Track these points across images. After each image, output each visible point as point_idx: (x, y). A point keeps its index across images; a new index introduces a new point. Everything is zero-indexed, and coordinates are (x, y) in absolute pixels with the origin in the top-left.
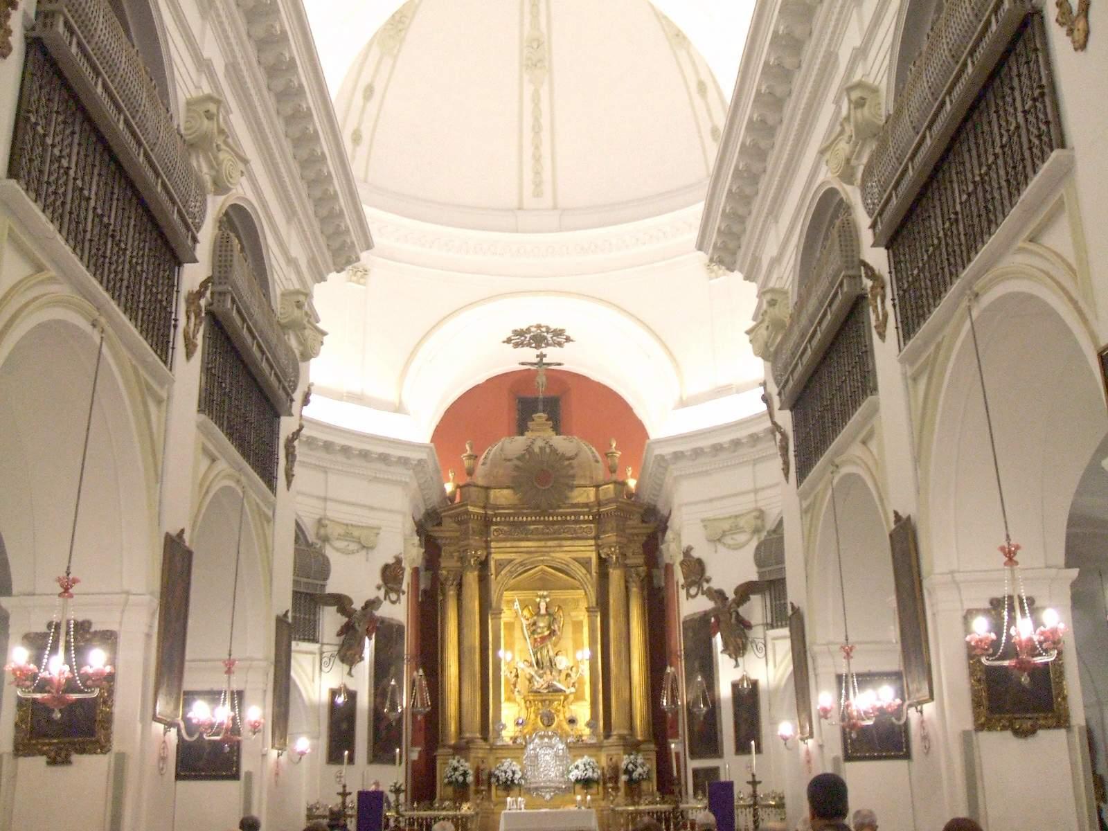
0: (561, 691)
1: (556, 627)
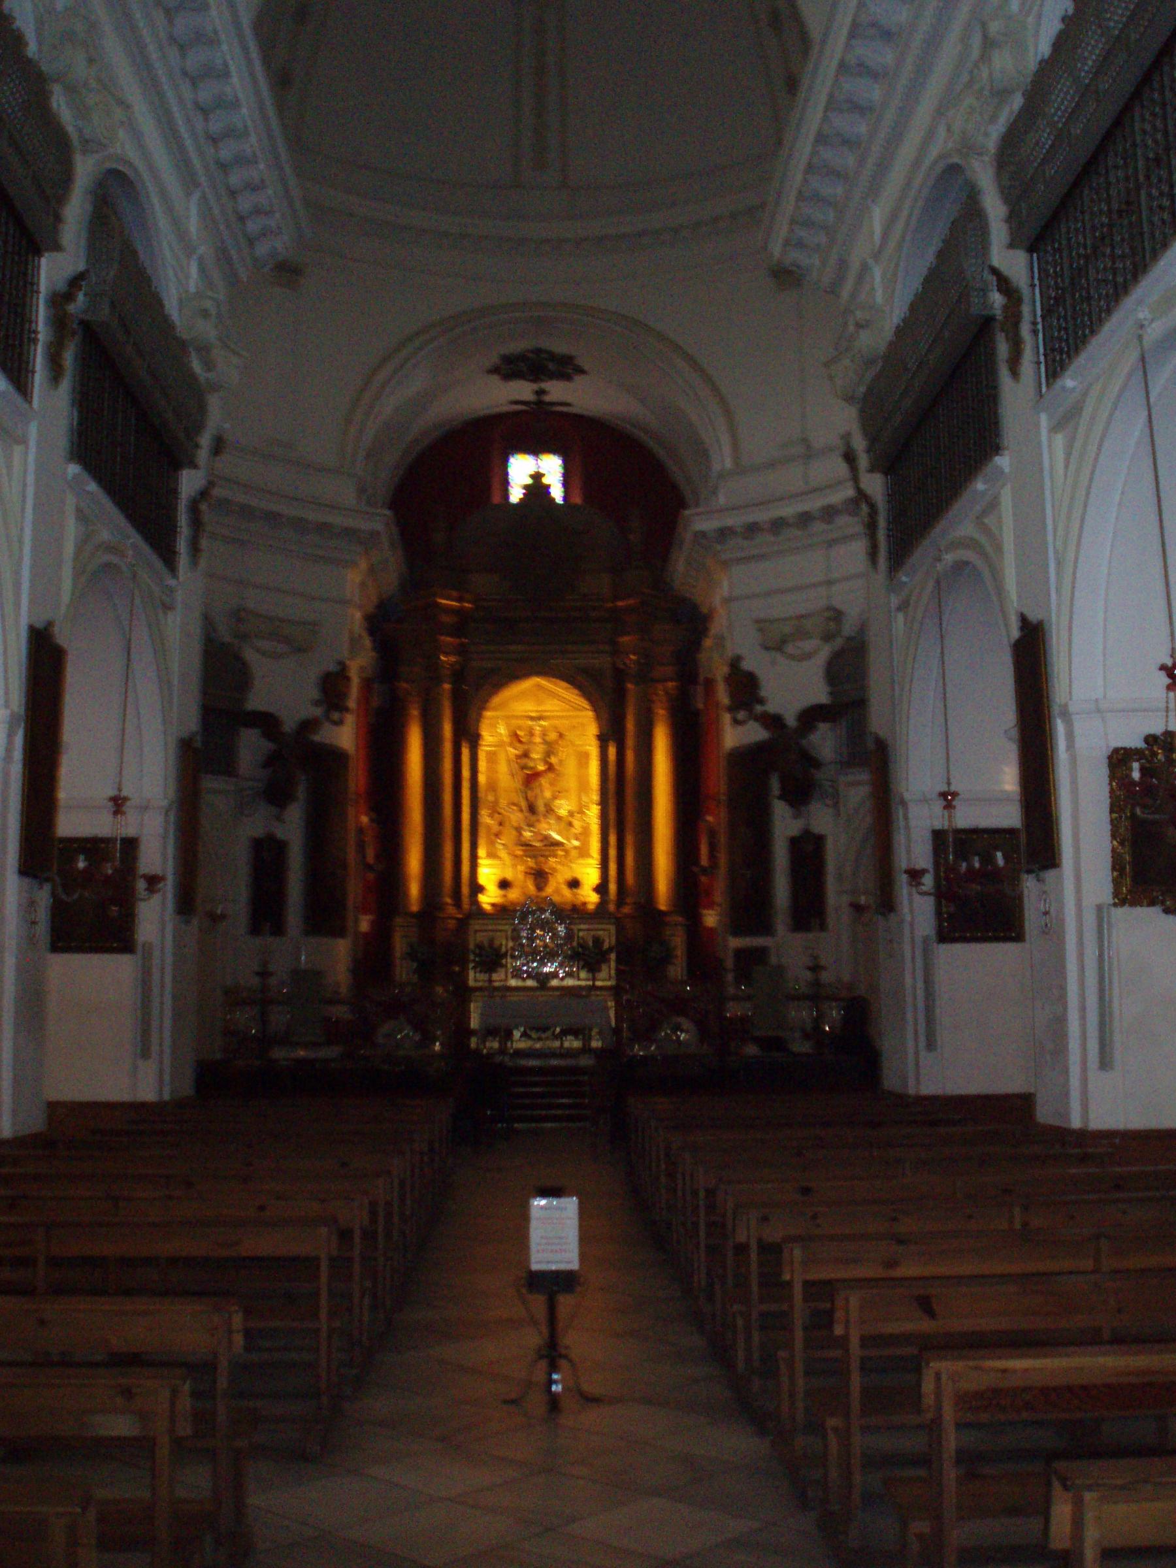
1: (553, 760)
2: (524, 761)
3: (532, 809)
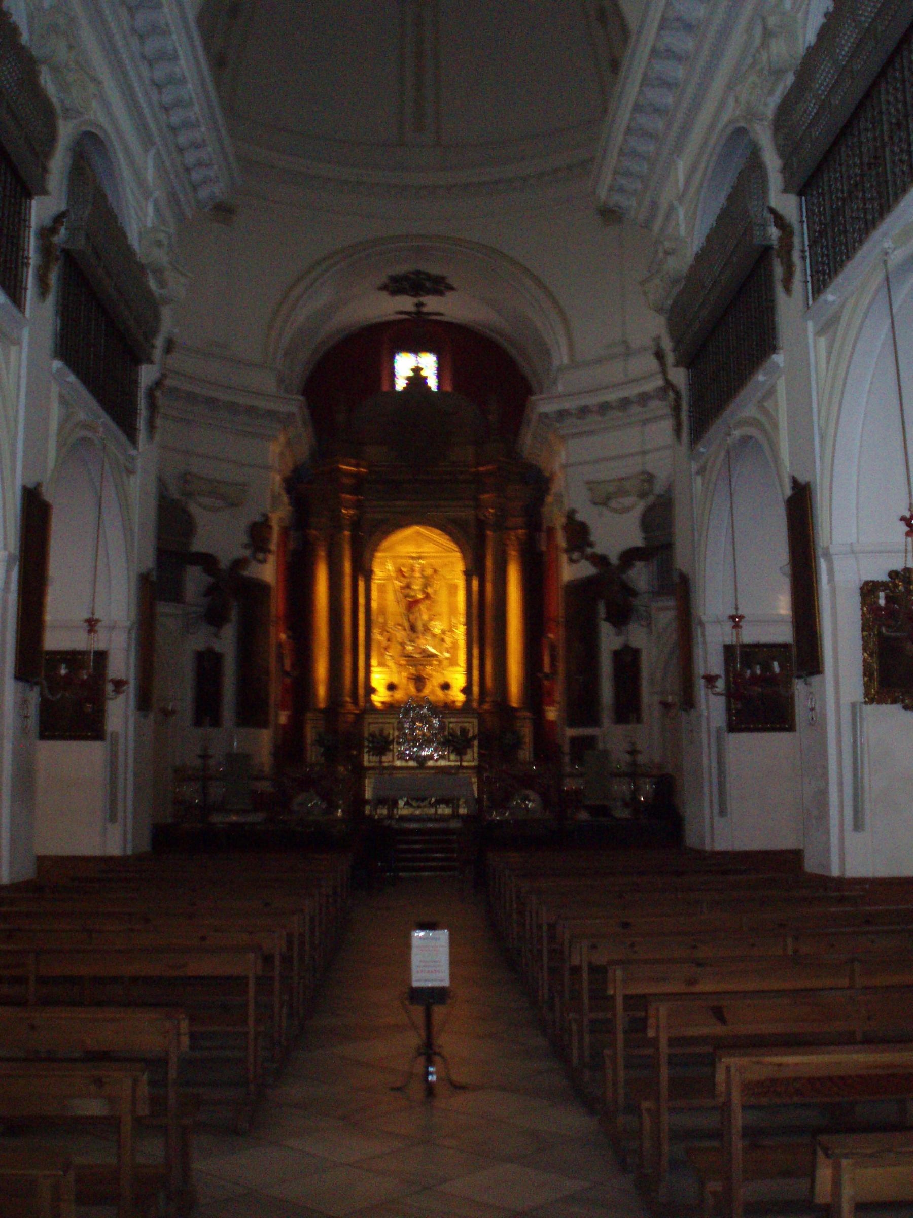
0: (433, 656)
1: (430, 590)
2: (407, 591)
3: (413, 628)
